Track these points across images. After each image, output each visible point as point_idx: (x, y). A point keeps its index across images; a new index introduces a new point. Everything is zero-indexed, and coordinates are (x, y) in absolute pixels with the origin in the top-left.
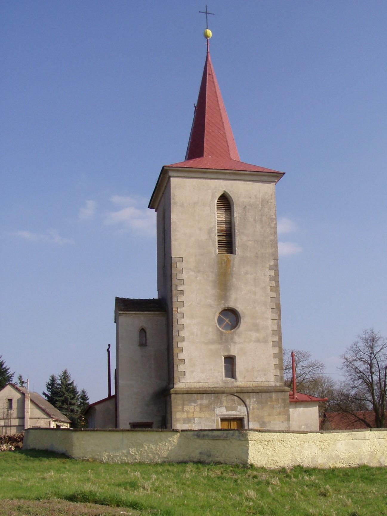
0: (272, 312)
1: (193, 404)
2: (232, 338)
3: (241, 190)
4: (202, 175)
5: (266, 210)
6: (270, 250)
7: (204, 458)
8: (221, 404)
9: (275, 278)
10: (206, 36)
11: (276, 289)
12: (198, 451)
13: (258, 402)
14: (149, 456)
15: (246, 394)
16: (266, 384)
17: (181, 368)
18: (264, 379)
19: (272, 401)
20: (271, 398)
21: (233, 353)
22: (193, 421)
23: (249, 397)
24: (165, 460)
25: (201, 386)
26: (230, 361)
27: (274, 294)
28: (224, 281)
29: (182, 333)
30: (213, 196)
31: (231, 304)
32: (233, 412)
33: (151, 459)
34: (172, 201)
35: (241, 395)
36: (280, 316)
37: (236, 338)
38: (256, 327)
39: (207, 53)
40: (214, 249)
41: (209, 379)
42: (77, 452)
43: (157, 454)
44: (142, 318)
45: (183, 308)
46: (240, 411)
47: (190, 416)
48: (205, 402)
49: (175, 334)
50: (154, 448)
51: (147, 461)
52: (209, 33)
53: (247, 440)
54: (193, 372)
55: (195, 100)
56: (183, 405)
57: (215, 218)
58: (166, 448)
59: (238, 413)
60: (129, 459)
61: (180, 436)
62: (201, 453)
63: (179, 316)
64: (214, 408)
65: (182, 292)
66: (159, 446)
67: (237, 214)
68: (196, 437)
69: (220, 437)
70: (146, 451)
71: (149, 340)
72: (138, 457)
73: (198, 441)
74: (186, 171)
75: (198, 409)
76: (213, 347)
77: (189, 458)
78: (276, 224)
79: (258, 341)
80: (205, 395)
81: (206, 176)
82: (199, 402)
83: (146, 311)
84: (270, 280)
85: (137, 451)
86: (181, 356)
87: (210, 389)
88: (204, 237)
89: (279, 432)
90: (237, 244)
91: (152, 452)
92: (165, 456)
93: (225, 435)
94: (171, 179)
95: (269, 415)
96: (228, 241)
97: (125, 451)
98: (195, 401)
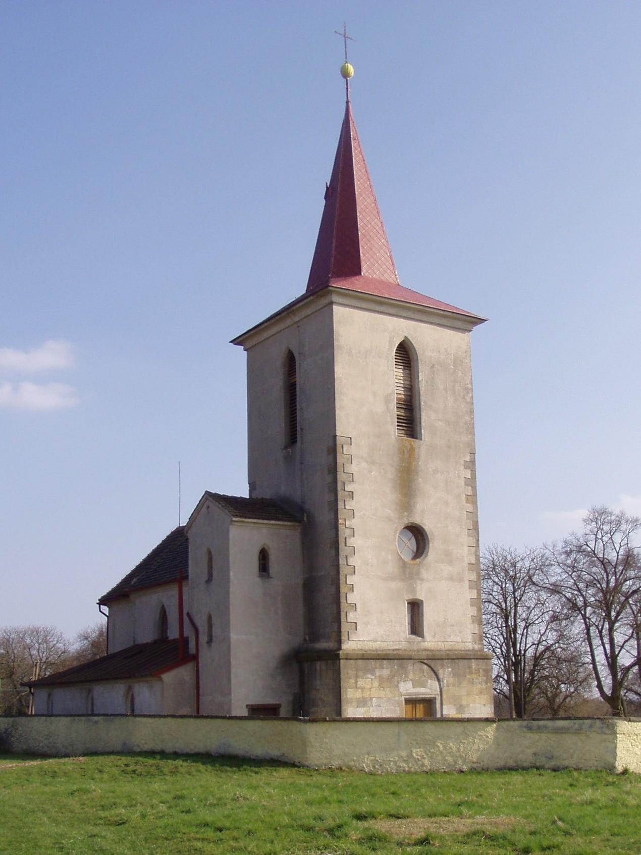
0: (469, 535)
1: (369, 676)
2: (418, 573)
3: (429, 339)
4: (377, 308)
5: (460, 374)
6: (466, 438)
7: (542, 761)
8: (406, 676)
9: (472, 482)
10: (345, 75)
11: (472, 499)
12: (530, 751)
13: (455, 674)
14: (446, 760)
15: (439, 662)
16: (461, 646)
17: (352, 617)
18: (459, 639)
19: (471, 673)
20: (470, 667)
21: (420, 596)
22: (369, 703)
23: (443, 666)
24: (475, 765)
25: (378, 647)
26: (415, 607)
27: (470, 507)
28: (406, 481)
29: (352, 561)
30: (391, 342)
31: (417, 520)
32: (422, 690)
33: (450, 765)
34: (336, 343)
35: (432, 661)
36: (478, 540)
37: (424, 574)
38: (448, 558)
39: (347, 102)
40: (392, 429)
41: (389, 636)
42: (315, 756)
43: (461, 757)
44: (265, 531)
45: (354, 520)
46: (430, 689)
47: (366, 694)
48: (386, 672)
49: (342, 561)
50: (454, 749)
51: (444, 768)
52: (351, 69)
53: (615, 733)
54: (367, 624)
55: (325, 175)
56: (357, 676)
57: (392, 378)
58: (476, 747)
59: (428, 691)
60: (410, 765)
61: (497, 729)
62: (535, 754)
63: (347, 532)
64: (398, 682)
65: (352, 494)
66: (464, 743)
67: (423, 376)
68: (525, 730)
69: (568, 729)
70: (441, 752)
71: (274, 567)
72: (426, 762)
73: (528, 735)
74: (438, 315)
75: (376, 684)
76: (394, 585)
77: (516, 762)
78: (472, 397)
79: (451, 578)
80: (385, 662)
81: (382, 309)
82: (378, 673)
83: (272, 519)
84: (466, 484)
85: (425, 752)
86: (352, 598)
87: (391, 652)
88: (380, 408)
89: (150, 716)
90: (423, 424)
91: (451, 754)
92: (475, 760)
93: (577, 726)
94: (334, 307)
95: (469, 694)
96: (410, 420)
97: (404, 754)
98: (372, 672)
